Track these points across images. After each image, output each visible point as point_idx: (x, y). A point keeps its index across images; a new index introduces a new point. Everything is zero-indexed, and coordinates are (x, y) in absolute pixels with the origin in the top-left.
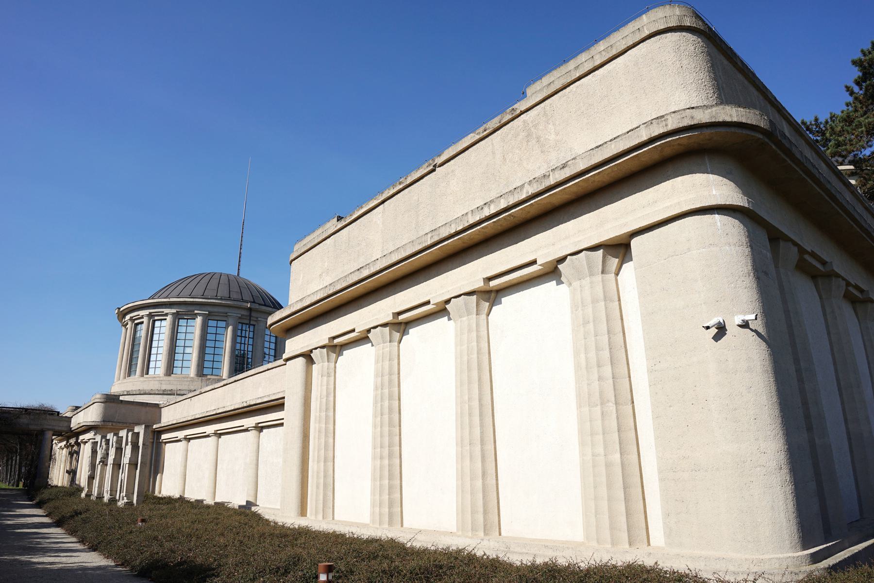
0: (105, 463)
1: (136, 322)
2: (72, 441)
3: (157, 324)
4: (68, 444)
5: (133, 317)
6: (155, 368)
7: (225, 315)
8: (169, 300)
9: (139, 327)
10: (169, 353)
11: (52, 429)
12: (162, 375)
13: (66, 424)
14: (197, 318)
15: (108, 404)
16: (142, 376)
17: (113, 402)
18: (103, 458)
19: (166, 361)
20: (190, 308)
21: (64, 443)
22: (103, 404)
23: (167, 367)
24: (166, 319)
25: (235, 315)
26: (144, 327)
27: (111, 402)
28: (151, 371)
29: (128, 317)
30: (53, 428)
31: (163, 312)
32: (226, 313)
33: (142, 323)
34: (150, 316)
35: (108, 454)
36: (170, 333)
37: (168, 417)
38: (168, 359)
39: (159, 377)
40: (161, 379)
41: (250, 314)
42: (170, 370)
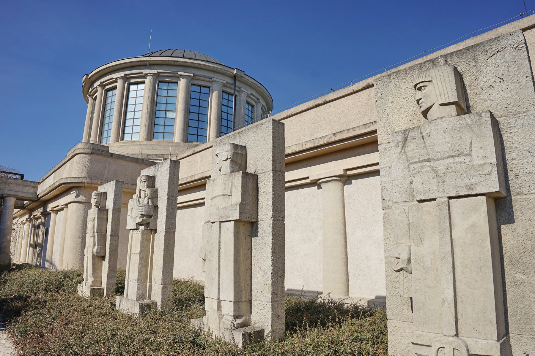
0: (151, 227)
1: (107, 87)
2: (38, 212)
3: (133, 88)
4: (32, 217)
5: (103, 82)
6: (132, 133)
7: (210, 80)
8: (150, 59)
9: (110, 93)
10: (150, 116)
11: (15, 195)
12: (143, 140)
13: (32, 190)
14: (180, 81)
15: (93, 156)
16: (117, 141)
17: (101, 155)
18: (147, 216)
19: (147, 125)
20: (173, 69)
21: (27, 216)
22: (87, 156)
23: (148, 132)
24: (143, 82)
25: (220, 81)
26: (118, 92)
27: (98, 154)
28: (127, 138)
29: (96, 84)
30: (16, 193)
31: (141, 73)
32: (211, 79)
33: (115, 88)
34: (126, 78)
35: (156, 207)
36: (150, 95)
37: (40, 241)
38: (149, 122)
39: (139, 141)
40: (142, 143)
41: (235, 82)
42: (151, 134)
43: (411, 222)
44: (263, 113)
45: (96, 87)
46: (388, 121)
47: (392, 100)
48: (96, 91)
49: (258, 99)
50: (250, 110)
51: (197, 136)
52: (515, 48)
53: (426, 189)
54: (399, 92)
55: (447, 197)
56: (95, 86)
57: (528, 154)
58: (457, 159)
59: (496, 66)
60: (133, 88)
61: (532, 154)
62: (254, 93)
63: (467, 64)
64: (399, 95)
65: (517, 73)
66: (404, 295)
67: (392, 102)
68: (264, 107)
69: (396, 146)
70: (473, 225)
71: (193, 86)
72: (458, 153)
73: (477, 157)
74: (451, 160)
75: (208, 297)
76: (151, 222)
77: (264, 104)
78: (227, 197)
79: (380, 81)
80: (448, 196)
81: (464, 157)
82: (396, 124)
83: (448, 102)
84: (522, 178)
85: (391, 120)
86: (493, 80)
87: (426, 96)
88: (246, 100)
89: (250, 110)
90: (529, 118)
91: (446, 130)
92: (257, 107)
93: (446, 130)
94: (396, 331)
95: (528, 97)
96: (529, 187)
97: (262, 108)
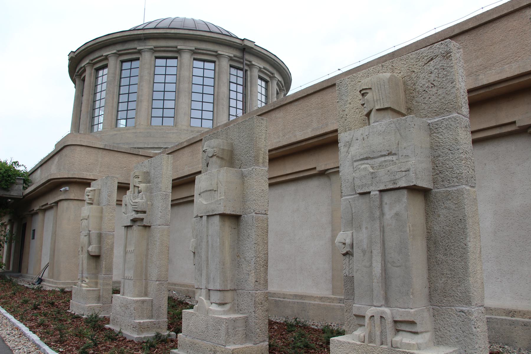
43: (353, 212)
44: (280, 90)
45: (84, 66)
46: (346, 121)
47: (350, 101)
48: (84, 71)
49: (272, 74)
50: (264, 87)
51: (201, 120)
52: (444, 56)
53: (363, 183)
54: (355, 94)
55: (378, 190)
56: (83, 65)
57: (450, 152)
58: (387, 158)
59: (430, 72)
60: (126, 65)
61: (452, 151)
62: (268, 67)
63: (408, 70)
64: (355, 96)
65: (444, 80)
66: (349, 275)
67: (350, 103)
68: (280, 82)
69: (345, 146)
70: (397, 214)
71: (195, 62)
72: (388, 152)
73: (402, 156)
74: (383, 159)
75: (198, 288)
76: (145, 218)
77: (280, 79)
78: (213, 192)
79: (341, 83)
80: (378, 190)
81: (392, 156)
82: (353, 124)
83: (383, 107)
84: (444, 173)
85: (349, 120)
86: (426, 85)
87: (368, 101)
88: (259, 75)
89: (264, 87)
90: (451, 120)
91: (380, 132)
92: (271, 83)
93: (380, 132)
94: (350, 310)
95: (451, 102)
96: (449, 180)
97: (278, 84)
